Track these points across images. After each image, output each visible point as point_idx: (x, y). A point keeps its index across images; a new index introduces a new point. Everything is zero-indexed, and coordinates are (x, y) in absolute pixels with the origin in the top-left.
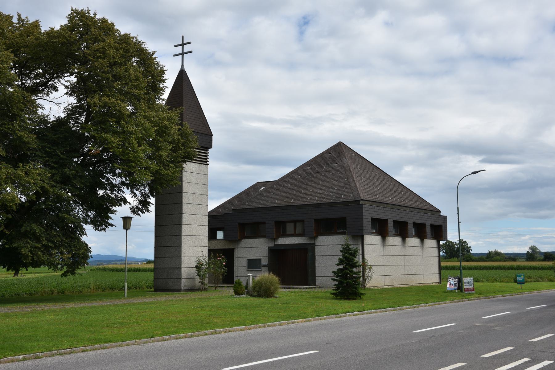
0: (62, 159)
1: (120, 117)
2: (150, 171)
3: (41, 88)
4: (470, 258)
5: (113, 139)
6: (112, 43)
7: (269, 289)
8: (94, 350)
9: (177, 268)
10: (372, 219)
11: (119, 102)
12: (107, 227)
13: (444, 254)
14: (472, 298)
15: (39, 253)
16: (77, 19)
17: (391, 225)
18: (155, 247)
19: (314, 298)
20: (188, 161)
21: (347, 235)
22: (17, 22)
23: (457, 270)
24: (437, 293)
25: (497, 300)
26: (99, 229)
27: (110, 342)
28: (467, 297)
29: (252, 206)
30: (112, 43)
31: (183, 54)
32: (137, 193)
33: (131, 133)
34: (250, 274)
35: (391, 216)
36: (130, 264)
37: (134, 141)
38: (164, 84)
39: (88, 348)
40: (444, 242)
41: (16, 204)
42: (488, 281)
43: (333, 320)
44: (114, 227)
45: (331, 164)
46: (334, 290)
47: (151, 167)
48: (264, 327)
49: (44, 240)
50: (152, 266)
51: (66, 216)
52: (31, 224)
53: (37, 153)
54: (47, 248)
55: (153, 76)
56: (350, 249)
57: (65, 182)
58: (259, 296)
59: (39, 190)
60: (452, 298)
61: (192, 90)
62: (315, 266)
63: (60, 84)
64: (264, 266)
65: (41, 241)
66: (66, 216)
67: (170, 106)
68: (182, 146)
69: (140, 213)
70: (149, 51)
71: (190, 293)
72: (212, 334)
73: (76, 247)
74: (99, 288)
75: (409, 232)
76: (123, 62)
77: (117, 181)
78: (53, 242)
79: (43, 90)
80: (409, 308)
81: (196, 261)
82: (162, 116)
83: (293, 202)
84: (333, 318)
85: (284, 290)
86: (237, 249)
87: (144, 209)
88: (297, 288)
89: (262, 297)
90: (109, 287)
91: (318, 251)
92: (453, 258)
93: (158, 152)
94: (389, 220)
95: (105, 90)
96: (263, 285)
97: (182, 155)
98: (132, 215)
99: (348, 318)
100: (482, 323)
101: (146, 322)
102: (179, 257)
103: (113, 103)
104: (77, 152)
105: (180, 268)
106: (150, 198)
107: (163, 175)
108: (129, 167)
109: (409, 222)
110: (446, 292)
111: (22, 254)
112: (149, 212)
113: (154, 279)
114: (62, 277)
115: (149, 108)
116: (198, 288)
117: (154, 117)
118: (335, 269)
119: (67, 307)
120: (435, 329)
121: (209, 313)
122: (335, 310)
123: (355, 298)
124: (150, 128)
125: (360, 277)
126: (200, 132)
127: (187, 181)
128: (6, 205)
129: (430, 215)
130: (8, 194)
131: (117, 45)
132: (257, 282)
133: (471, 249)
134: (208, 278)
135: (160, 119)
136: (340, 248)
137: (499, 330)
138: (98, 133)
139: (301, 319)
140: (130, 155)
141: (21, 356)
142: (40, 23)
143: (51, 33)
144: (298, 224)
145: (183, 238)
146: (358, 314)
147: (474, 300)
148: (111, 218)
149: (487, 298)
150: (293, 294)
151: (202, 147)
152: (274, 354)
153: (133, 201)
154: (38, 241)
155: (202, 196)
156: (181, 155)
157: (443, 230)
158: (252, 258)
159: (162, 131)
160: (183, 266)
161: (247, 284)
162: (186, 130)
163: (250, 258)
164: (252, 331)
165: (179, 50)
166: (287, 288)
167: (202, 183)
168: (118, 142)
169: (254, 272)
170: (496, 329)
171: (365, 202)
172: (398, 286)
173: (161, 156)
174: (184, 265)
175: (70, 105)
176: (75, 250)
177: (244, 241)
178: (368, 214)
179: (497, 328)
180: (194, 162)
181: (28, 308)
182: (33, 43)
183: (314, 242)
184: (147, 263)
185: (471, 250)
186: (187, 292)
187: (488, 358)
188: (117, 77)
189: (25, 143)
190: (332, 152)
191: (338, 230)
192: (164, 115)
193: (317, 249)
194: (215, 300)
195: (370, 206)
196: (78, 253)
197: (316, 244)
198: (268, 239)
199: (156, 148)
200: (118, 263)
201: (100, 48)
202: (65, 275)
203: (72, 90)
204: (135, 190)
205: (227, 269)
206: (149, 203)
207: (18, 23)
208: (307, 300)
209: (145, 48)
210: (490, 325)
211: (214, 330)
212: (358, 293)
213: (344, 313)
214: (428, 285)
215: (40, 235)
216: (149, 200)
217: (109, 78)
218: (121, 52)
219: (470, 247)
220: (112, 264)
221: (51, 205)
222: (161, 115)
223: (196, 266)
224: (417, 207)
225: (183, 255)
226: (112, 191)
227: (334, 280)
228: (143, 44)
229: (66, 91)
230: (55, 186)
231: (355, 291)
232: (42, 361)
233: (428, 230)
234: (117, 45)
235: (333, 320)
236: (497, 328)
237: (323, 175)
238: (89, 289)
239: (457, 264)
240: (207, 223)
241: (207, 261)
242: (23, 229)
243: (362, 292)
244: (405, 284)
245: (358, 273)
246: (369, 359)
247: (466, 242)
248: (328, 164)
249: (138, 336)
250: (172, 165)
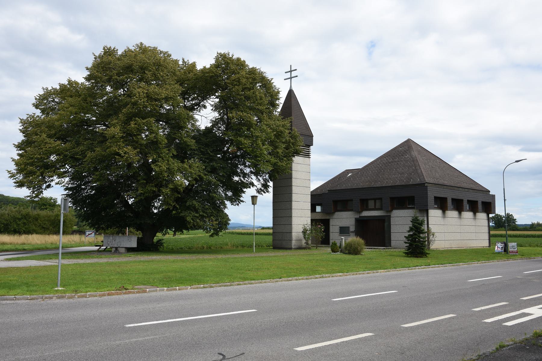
0: (211, 156)
1: (249, 125)
2: (270, 163)
3: (195, 107)
4: (516, 228)
5: (245, 141)
6: (244, 74)
7: (357, 249)
8: (245, 284)
10: (435, 197)
11: (249, 115)
12: (239, 203)
13: (493, 224)
14: (515, 258)
15: (198, 220)
16: (221, 59)
17: (449, 202)
18: (273, 217)
19: (391, 256)
20: (296, 156)
21: (416, 209)
22: (182, 63)
23: (504, 237)
24: (487, 254)
25: (536, 260)
26: (235, 204)
27: (254, 280)
28: (511, 258)
29: (343, 188)
30: (244, 74)
31: (291, 78)
32: (261, 179)
34: (343, 238)
35: (449, 195)
36: (249, 229)
37: (260, 142)
38: (279, 101)
39: (241, 283)
40: (493, 215)
41: (183, 187)
42: (530, 246)
43: (406, 271)
44: (244, 203)
45: (403, 155)
46: (406, 250)
47: (271, 161)
48: (357, 274)
49: (200, 212)
50: (271, 231)
51: (215, 195)
52: (192, 201)
53: (196, 152)
54: (202, 216)
55: (272, 96)
56: (418, 220)
57: (213, 171)
58: (349, 253)
59: (198, 178)
60: (500, 258)
61: (298, 104)
62: (391, 233)
63: (208, 104)
65: (199, 212)
66: (215, 195)
67: (283, 117)
68: (292, 145)
69: (263, 193)
70: (269, 78)
71: (299, 250)
72: (320, 278)
73: (221, 216)
74: (234, 246)
75: (464, 207)
76: (252, 87)
77: (247, 170)
78: (206, 213)
79: (197, 108)
80: (465, 265)
82: (278, 124)
84: (406, 270)
85: (368, 250)
87: (265, 190)
88: (377, 249)
89: (352, 254)
90: (240, 245)
91: (393, 221)
92: (501, 228)
93: (276, 150)
94: (448, 198)
95: (240, 107)
96: (353, 246)
97: (292, 152)
98: (257, 195)
99: (417, 270)
100: (523, 276)
101: (273, 268)
103: (245, 116)
104: (220, 151)
105: (291, 233)
106: (269, 182)
107: (279, 166)
108: (257, 161)
109: (464, 200)
110: (494, 254)
111: (187, 221)
112: (268, 192)
113: (273, 240)
114: (210, 237)
115: (269, 118)
116: (304, 247)
117: (273, 125)
118: (407, 235)
119: (218, 257)
120: (485, 279)
121: (316, 264)
122: (407, 264)
123: (422, 256)
124: (271, 133)
125: (425, 241)
127: (295, 170)
128: (177, 188)
129: (481, 194)
130: (178, 181)
131: (247, 75)
132: (348, 243)
133: (516, 221)
134: (311, 240)
135: (277, 127)
136: (410, 219)
137: (536, 282)
138: (235, 138)
139: (383, 270)
140: (257, 152)
141: (202, 285)
142: (196, 63)
143: (204, 70)
144: (377, 201)
145: (293, 211)
146: (425, 268)
147: (517, 260)
148: (242, 197)
149: (528, 259)
150: (374, 252)
151: (306, 145)
152: (366, 292)
153: (258, 185)
154: (197, 212)
156: (291, 151)
157: (492, 206)
158: (343, 226)
159: (279, 135)
160: (293, 231)
161: (341, 245)
162: (295, 133)
163: (341, 226)
164: (348, 277)
165: (288, 75)
166: (369, 248)
168: (249, 143)
169: (345, 236)
170: (534, 281)
171: (429, 184)
172: (456, 249)
173: (278, 153)
175: (215, 118)
176: (221, 219)
177: (337, 213)
178: (432, 193)
179: (535, 280)
180: (301, 156)
181: (194, 257)
182: (192, 77)
183: (389, 215)
184: (262, 229)
185: (517, 222)
186: (296, 249)
187: (526, 300)
188: (248, 98)
189: (188, 146)
190: (403, 146)
191: (408, 205)
192: (280, 123)
193: (392, 220)
194: (318, 255)
195: (433, 188)
196: (222, 221)
197: (391, 216)
199: (274, 146)
200: (240, 228)
201: (236, 79)
202: (212, 236)
203: (216, 108)
204: (259, 177)
205: (325, 233)
206: (268, 186)
207: (183, 65)
208: (385, 257)
209: (266, 76)
210: (530, 278)
211: (322, 275)
212: (425, 252)
213: (414, 267)
214: (480, 248)
215: (198, 208)
216: (268, 184)
217: (242, 99)
218: (250, 80)
219: (516, 219)
220: (236, 229)
221: (205, 188)
222: (277, 124)
223: (303, 231)
224: (471, 188)
225: (293, 223)
226: (244, 177)
227: (406, 243)
228: (265, 73)
229: (211, 108)
230: (207, 175)
231: (422, 251)
232: (215, 289)
233: (480, 206)
234: (247, 75)
235: (406, 271)
236: (535, 280)
237: (396, 164)
238: (227, 246)
239: (504, 232)
240: (310, 200)
241: (310, 228)
242: (188, 204)
243: (427, 252)
244: (461, 247)
245: (424, 238)
246: (435, 298)
247: (512, 215)
249: (271, 277)
250: (285, 159)
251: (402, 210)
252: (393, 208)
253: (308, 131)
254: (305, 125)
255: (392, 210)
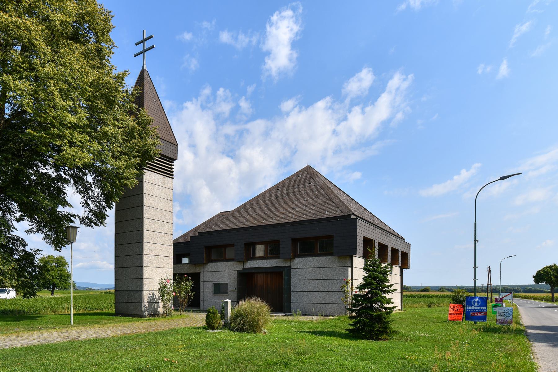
9: (138, 291)
33: (49, 77)
64: (232, 291)
81: (159, 284)
83: (263, 223)
86: (203, 273)
91: (294, 274)
102: (140, 278)
126: (163, 138)
145: (145, 257)
155: (166, 212)
158: (219, 282)
163: (217, 282)
167: (166, 198)
174: (145, 288)
183: (289, 265)
197: (292, 267)
198: (236, 262)
225: (144, 277)
248: (299, 185)
251: (309, 258)
252: (296, 256)
253: (169, 136)
254: (166, 127)
255: (294, 258)
